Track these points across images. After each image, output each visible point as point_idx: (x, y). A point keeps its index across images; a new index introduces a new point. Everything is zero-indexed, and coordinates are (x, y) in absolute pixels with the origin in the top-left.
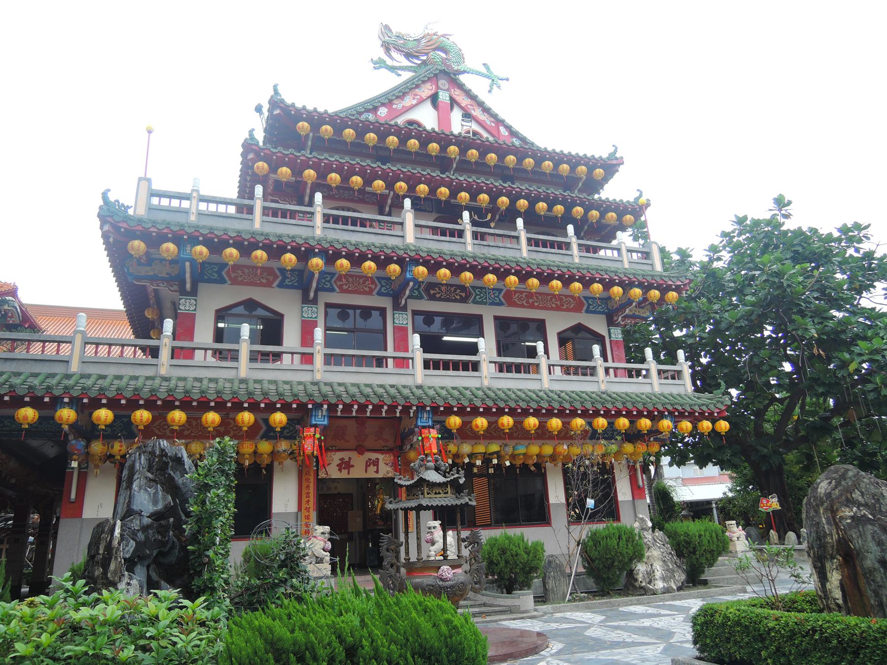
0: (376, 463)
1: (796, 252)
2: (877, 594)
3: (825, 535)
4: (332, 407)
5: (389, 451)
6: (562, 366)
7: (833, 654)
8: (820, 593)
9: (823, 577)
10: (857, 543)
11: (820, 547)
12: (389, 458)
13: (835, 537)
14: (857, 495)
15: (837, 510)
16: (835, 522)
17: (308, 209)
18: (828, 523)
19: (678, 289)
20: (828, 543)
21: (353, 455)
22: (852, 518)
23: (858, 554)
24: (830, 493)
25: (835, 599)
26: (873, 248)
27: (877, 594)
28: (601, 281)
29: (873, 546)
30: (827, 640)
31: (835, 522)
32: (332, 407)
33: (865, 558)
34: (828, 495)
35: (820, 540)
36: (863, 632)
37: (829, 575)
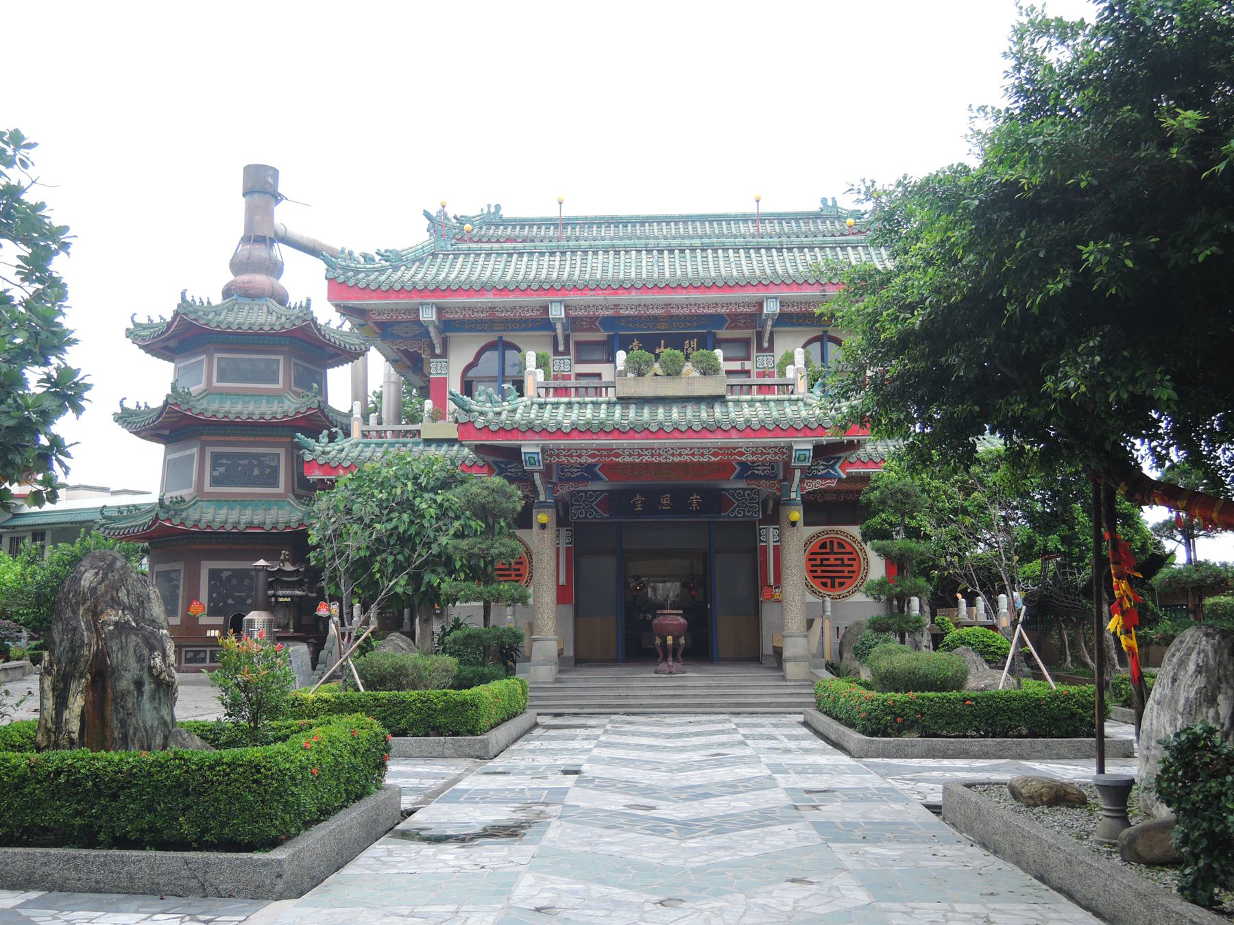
2: (123, 724)
3: (81, 647)
7: (78, 802)
8: (50, 725)
9: (61, 703)
10: (115, 658)
11: (70, 661)
13: (94, 648)
14: (122, 594)
15: (102, 612)
16: (96, 628)
17: (781, 466)
18: (88, 629)
20: (82, 656)
22: (116, 624)
23: (113, 672)
24: (95, 588)
25: (70, 733)
26: (25, 183)
27: (123, 724)
29: (133, 664)
30: (76, 783)
31: (96, 628)
33: (120, 677)
34: (93, 590)
35: (74, 652)
36: (133, 767)
37: (71, 699)
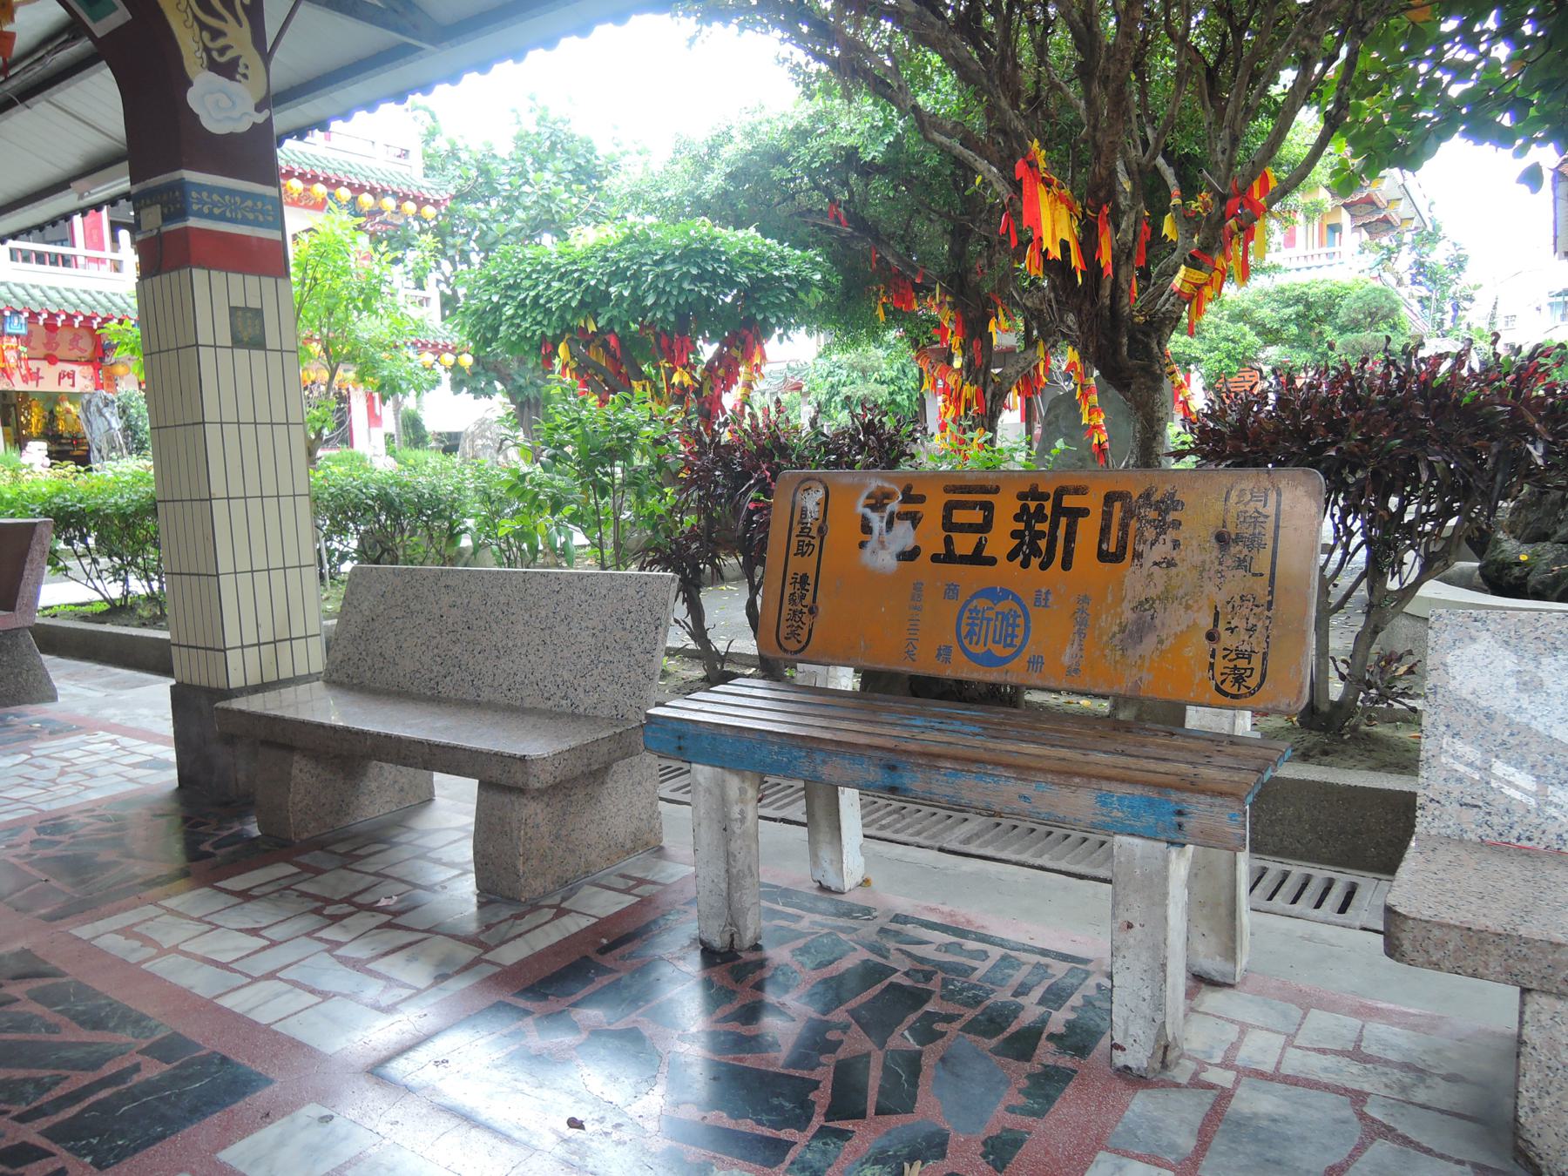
0: (71, 375)
1: (579, 165)
4: (34, 316)
5: (88, 362)
6: (814, 1137)
12: (89, 370)
19: (436, 204)
21: (44, 365)
28: (350, 186)
32: (34, 316)
